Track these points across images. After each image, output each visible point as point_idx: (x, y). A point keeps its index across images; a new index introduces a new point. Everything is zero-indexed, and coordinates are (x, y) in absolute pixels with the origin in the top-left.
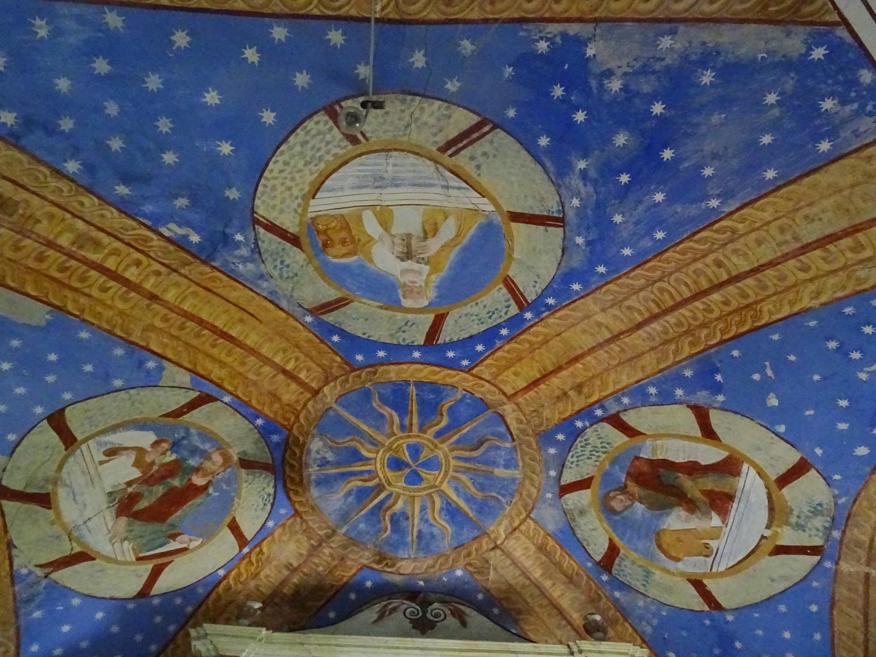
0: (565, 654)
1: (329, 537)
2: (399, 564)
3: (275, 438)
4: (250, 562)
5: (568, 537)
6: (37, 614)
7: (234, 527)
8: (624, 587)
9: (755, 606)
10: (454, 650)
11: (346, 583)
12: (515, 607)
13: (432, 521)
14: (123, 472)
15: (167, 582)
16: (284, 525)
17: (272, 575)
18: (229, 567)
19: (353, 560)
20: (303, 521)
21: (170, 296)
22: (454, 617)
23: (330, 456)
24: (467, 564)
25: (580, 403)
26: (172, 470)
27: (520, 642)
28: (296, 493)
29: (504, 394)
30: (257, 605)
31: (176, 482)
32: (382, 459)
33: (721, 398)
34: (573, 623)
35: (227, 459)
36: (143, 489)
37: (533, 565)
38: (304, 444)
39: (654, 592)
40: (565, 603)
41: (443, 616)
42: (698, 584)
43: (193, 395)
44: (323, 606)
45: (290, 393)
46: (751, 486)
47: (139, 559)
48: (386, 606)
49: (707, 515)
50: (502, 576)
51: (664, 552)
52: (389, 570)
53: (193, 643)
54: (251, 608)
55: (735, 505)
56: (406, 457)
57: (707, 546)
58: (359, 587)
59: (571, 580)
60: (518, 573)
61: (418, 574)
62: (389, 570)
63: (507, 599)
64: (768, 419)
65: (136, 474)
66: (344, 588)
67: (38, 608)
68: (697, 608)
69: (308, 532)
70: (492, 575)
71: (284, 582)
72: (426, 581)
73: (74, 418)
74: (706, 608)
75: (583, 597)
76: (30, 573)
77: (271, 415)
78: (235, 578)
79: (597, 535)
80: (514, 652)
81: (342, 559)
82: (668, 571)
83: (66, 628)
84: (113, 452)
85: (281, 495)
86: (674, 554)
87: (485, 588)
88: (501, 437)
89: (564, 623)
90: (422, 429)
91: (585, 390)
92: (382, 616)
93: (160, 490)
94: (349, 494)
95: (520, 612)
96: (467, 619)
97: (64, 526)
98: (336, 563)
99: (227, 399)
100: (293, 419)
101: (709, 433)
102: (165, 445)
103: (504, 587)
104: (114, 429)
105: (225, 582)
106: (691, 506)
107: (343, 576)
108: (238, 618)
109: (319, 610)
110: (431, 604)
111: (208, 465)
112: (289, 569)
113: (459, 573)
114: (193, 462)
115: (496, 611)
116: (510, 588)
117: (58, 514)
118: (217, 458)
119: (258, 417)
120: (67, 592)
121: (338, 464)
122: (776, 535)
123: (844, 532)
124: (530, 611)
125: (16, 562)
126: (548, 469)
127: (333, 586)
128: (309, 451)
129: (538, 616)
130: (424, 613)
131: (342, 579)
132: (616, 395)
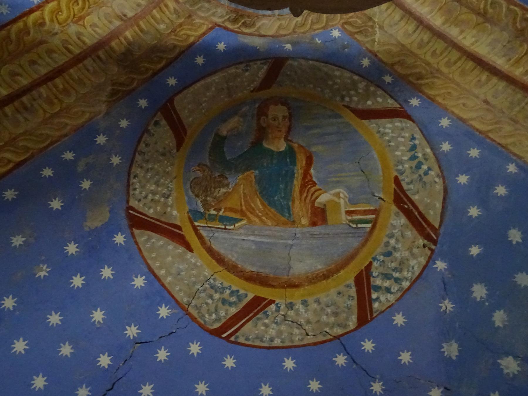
2: (258, 24)
11: (193, 44)
12: (413, 71)
17: (100, 24)
19: (202, 18)
24: (345, 23)
37: (431, 12)
40: (482, 50)
44: (163, 69)
50: (391, 35)
52: (247, 31)
58: (207, 50)
60: (411, 27)
61: (282, 36)
62: (247, 31)
63: (401, 63)
66: (190, 50)
70: (378, 36)
71: (114, 35)
72: (293, 44)
75: (506, 35)
78: (52, 12)
81: (190, 16)
87: (371, 52)
95: (420, 77)
98: (182, 20)
103: (394, 49)
105: (37, 14)
107: (189, 36)
109: (155, 74)
112: (122, 19)
113: (336, 33)
115: (388, 79)
116: (403, 49)
124: (435, 73)
127: (175, 47)
131: (186, 39)
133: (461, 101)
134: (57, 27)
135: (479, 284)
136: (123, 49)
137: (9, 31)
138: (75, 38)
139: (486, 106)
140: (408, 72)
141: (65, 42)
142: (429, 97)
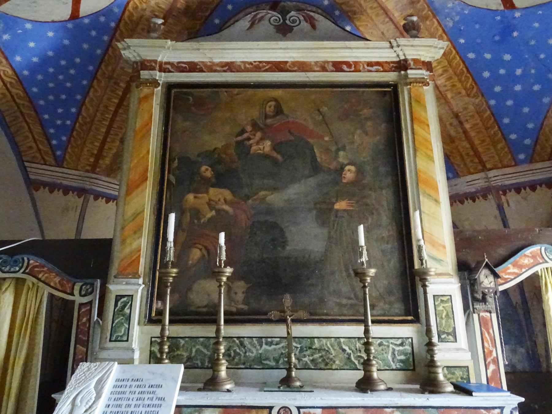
0: (387, 48)
10: (308, 49)
22: (307, 22)
27: (354, 40)
30: (160, 21)
34: (394, 20)
41: (298, 22)
53: (122, 52)
54: (155, 24)
68: (494, 8)
80: (350, 48)
89: (387, 19)
92: (253, 24)
95: (355, 13)
96: (317, 23)
108: (149, 32)
110: (289, 12)
124: (363, 12)
129: (368, 15)
130: (284, 20)
133: (371, 31)
134: (144, 5)
135: (220, 367)
136: (184, 6)
137: (124, 20)
138: (156, 7)
139: (382, 36)
140: (348, 9)
141: (152, 11)
142: (356, 26)
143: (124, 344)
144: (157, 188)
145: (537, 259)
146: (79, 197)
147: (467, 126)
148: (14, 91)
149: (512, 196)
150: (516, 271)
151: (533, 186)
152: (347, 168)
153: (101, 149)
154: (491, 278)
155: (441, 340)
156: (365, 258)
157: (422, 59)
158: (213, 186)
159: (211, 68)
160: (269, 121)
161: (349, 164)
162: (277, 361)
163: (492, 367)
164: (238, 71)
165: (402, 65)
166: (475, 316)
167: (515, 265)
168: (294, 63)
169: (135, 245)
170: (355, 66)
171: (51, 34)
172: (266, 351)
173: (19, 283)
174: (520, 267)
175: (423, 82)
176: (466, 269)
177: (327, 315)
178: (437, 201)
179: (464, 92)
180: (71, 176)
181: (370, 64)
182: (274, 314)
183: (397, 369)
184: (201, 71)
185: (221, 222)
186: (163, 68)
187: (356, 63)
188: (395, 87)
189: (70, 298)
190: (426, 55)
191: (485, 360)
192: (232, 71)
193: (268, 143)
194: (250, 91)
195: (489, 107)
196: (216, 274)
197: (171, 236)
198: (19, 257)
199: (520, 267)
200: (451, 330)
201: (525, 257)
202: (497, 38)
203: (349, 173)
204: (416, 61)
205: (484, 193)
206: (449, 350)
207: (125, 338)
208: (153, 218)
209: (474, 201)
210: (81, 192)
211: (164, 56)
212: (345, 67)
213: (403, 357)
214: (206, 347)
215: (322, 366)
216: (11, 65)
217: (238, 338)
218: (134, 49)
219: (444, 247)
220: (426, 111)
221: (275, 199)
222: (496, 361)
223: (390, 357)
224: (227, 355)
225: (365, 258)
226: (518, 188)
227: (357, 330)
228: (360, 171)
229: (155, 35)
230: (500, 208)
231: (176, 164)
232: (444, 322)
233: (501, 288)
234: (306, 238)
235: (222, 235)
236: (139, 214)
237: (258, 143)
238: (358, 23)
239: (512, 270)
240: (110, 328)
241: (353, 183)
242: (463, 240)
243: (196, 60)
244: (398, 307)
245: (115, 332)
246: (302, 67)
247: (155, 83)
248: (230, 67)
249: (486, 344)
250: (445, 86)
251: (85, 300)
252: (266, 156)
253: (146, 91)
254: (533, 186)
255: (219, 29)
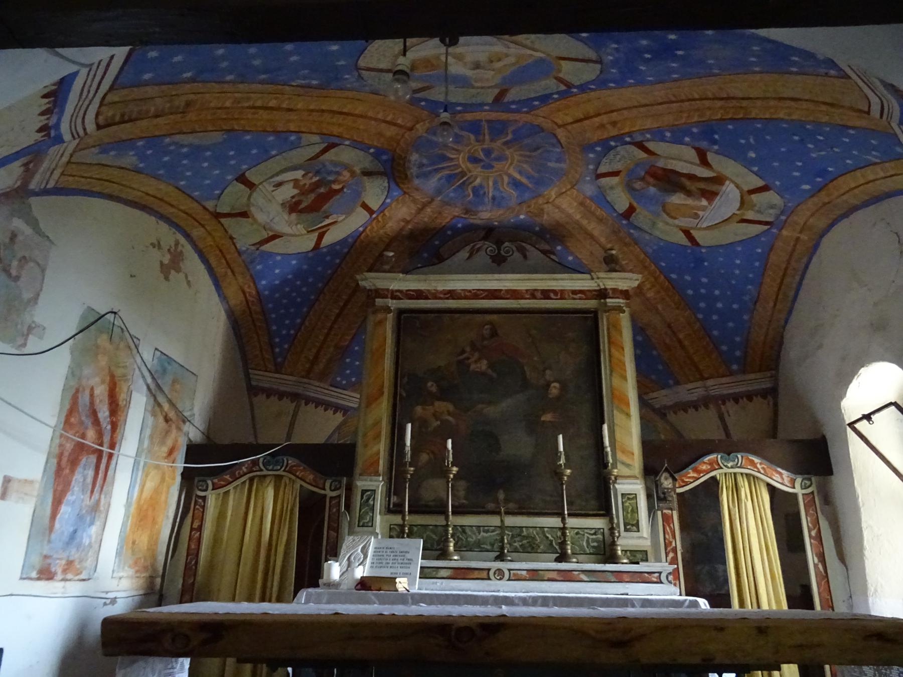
1: (430, 203)
3: (384, 157)
4: (379, 221)
5: (601, 198)
6: (259, 267)
7: (365, 206)
8: (636, 228)
9: (721, 246)
13: (501, 189)
14: (288, 192)
15: (328, 240)
16: (397, 200)
18: (365, 226)
20: (410, 196)
21: (300, 106)
23: (425, 161)
25: (614, 132)
26: (317, 185)
28: (403, 183)
29: (556, 123)
31: (322, 190)
32: (463, 158)
33: (716, 147)
35: (353, 174)
36: (302, 198)
38: (406, 157)
39: (657, 233)
40: (596, 233)
42: (687, 233)
43: (324, 146)
45: (391, 131)
46: (730, 194)
47: (308, 232)
48: (474, 246)
49: (699, 199)
51: (668, 214)
54: (388, 257)
55: (718, 197)
56: (482, 155)
57: (696, 214)
58: (454, 228)
59: (600, 220)
64: (749, 164)
65: (296, 191)
66: (443, 229)
67: (259, 264)
69: (414, 201)
70: (545, 217)
71: (402, 229)
73: (251, 176)
74: (689, 244)
76: (248, 249)
77: (379, 145)
79: (621, 200)
82: (667, 224)
83: (277, 271)
84: (279, 185)
85: (393, 186)
86: (673, 214)
88: (553, 145)
90: (492, 140)
91: (619, 125)
93: (312, 196)
94: (440, 179)
95: (564, 236)
97: (260, 224)
99: (347, 143)
100: (395, 145)
101: (704, 162)
102: (310, 175)
104: (277, 174)
106: (689, 193)
111: (341, 178)
113: (522, 217)
114: (331, 178)
115: (548, 236)
117: (255, 220)
118: (346, 175)
119: (369, 148)
120: (271, 255)
121: (431, 165)
122: (743, 214)
123: (788, 218)
125: (238, 246)
126: (588, 165)
128: (409, 161)
130: (499, 250)
132: (642, 132)
134: (374, 234)
143: (370, 529)
144: (391, 400)
145: (714, 465)
146: (292, 402)
147: (681, 336)
148: (253, 308)
149: (730, 406)
150: (695, 475)
151: (750, 396)
152: (553, 385)
153: (316, 357)
154: (670, 480)
155: (626, 530)
156: (562, 461)
157: (620, 288)
158: (439, 399)
159: (435, 295)
160: (485, 342)
161: (553, 382)
162: (492, 545)
163: (671, 555)
164: (459, 299)
165: (602, 294)
166: (659, 513)
167: (695, 470)
168: (508, 291)
169: (375, 449)
170: (561, 294)
171: (294, 262)
172: (483, 537)
173: (279, 478)
174: (699, 472)
175: (620, 310)
176: (650, 472)
177: (534, 509)
178: (628, 415)
179: (673, 305)
180: (287, 382)
181: (574, 292)
182: (491, 506)
183: (590, 554)
184: (427, 298)
185: (446, 431)
186: (394, 295)
187: (562, 291)
188: (595, 313)
189: (322, 492)
190: (623, 285)
191: (666, 549)
192: (454, 299)
193: (485, 362)
194: (468, 316)
195: (698, 319)
196: (445, 473)
197: (408, 443)
198: (280, 458)
199: (699, 472)
200: (635, 522)
201: (704, 463)
202: (692, 265)
203: (555, 389)
204: (615, 290)
205: (705, 402)
206: (633, 538)
207: (370, 524)
208: (389, 428)
209: (697, 410)
210: (295, 397)
211: (394, 286)
212: (552, 295)
213: (595, 544)
214: (435, 533)
215: (529, 550)
216: (256, 287)
217: (461, 526)
218: (372, 280)
219: (633, 454)
220: (621, 336)
221: (492, 411)
222: (675, 550)
223: (585, 544)
224: (452, 536)
225: (562, 461)
226: (736, 398)
227: (555, 522)
228: (564, 388)
229: (387, 267)
230: (722, 418)
231: (406, 379)
232: (629, 515)
233: (679, 490)
234: (517, 445)
235: (450, 442)
236: (377, 423)
237: (476, 362)
238: (569, 244)
239: (692, 474)
240: (358, 515)
241: (558, 398)
242: (647, 446)
243: (422, 288)
244: (593, 503)
245: (363, 519)
246: (515, 294)
247: (387, 310)
248: (451, 294)
249: (667, 536)
250: (655, 299)
251: (334, 494)
252: (483, 374)
253: (380, 316)
254: (750, 396)
255: (441, 259)
